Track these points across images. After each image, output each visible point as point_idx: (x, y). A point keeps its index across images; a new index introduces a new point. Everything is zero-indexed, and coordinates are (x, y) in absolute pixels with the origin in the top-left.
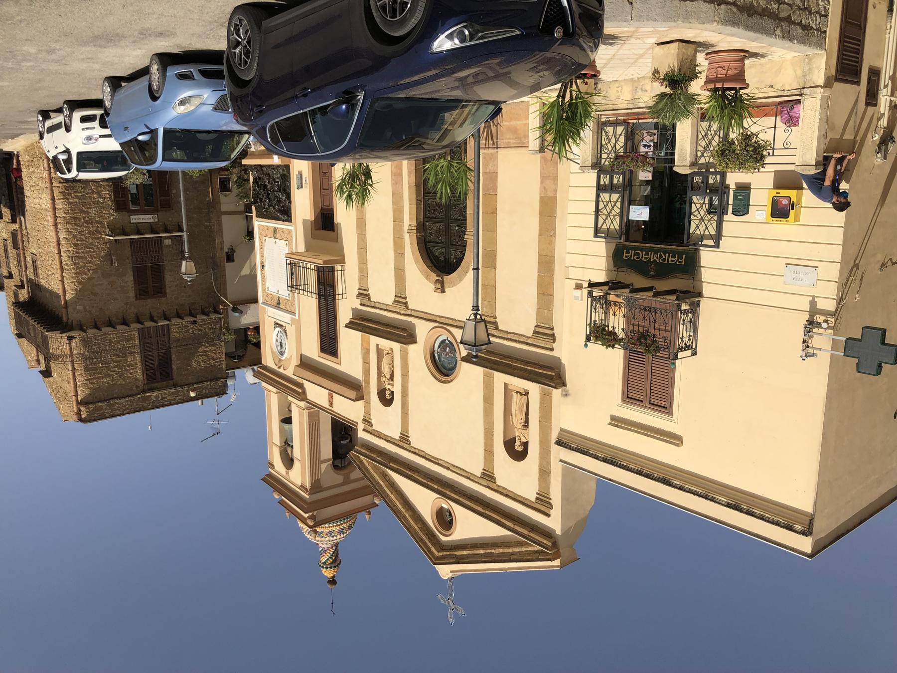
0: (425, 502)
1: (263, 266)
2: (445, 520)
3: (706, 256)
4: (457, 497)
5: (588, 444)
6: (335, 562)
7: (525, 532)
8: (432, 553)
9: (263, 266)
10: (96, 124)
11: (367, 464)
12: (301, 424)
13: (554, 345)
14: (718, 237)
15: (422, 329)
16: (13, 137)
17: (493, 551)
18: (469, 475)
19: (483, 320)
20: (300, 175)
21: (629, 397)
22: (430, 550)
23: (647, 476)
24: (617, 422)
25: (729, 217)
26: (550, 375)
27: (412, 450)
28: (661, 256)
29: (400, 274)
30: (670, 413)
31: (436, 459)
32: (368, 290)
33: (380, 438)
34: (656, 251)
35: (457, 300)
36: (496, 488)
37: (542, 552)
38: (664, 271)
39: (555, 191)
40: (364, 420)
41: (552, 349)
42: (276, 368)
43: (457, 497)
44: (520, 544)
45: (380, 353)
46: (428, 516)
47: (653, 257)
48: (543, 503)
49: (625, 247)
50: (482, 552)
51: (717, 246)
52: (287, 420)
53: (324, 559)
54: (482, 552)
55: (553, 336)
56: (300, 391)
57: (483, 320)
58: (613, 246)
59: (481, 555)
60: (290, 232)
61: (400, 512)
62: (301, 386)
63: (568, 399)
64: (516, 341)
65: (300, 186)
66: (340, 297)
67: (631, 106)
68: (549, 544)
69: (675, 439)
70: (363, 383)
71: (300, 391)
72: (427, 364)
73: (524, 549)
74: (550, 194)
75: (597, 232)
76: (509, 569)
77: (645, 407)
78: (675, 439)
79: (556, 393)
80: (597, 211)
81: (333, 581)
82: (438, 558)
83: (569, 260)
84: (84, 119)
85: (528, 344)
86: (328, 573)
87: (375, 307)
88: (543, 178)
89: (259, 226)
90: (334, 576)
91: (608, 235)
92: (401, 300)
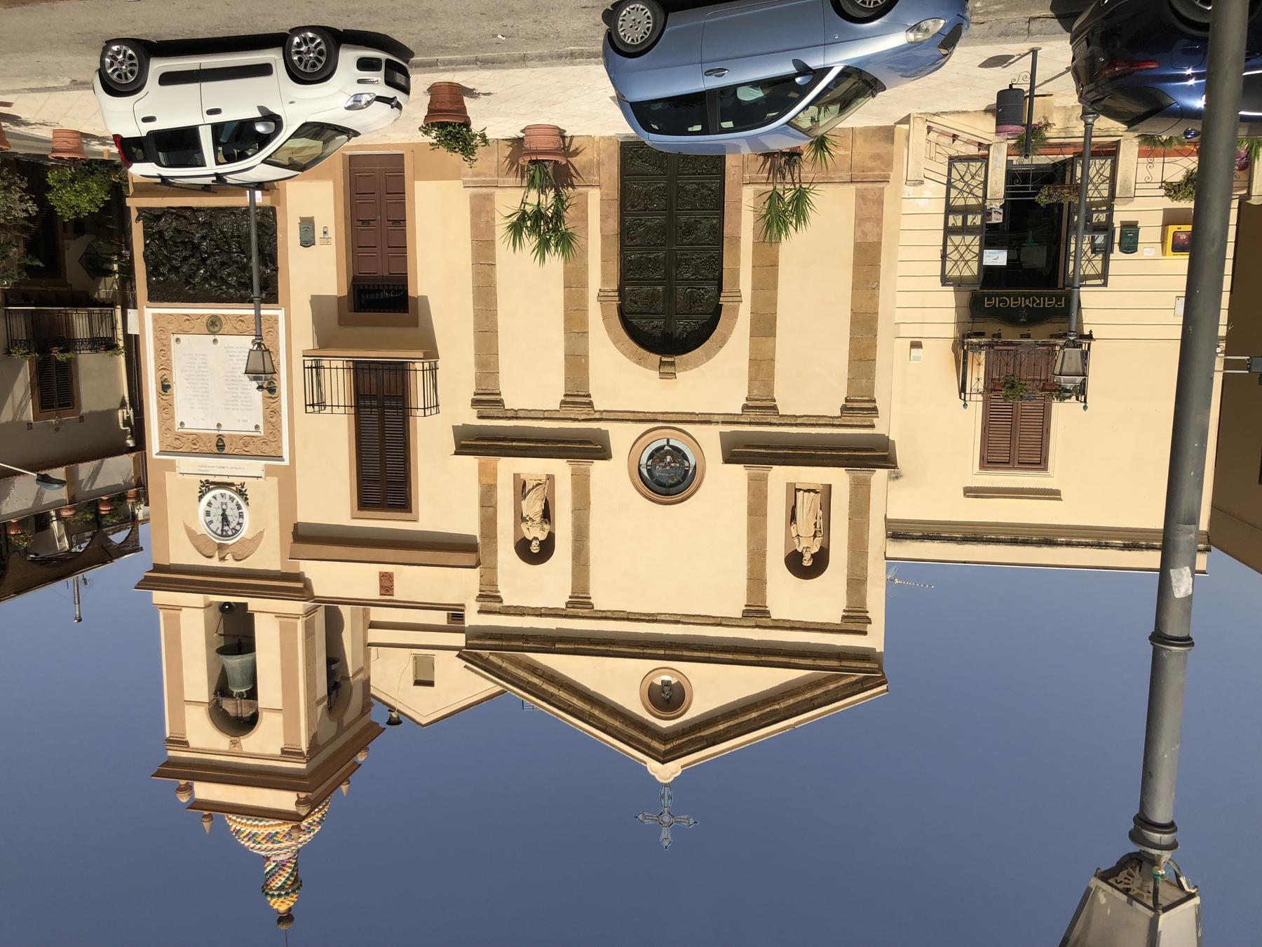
0: (622, 682)
1: (165, 387)
2: (668, 698)
3: (1089, 298)
4: (707, 655)
5: (935, 529)
6: (296, 883)
7: (835, 663)
8: (654, 750)
9: (165, 387)
10: (378, 76)
11: (498, 661)
12: (353, 629)
13: (875, 420)
14: (1104, 275)
15: (622, 437)
16: (486, 63)
17: (703, 734)
18: (718, 621)
19: (761, 405)
20: (307, 226)
21: (988, 462)
22: (649, 747)
23: (1025, 543)
24: (970, 492)
25: (1116, 254)
26: (873, 455)
27: (599, 615)
28: (1034, 301)
29: (576, 363)
30: (1045, 469)
31: (653, 615)
32: (499, 394)
33: (523, 615)
34: (1027, 296)
35: (713, 382)
36: (771, 624)
37: (865, 679)
38: (1036, 317)
39: (880, 235)
40: (482, 597)
41: (873, 426)
42: (215, 562)
43: (707, 655)
44: (829, 680)
45: (522, 489)
46: (634, 703)
47: (1023, 302)
48: (856, 619)
49: (984, 295)
50: (754, 715)
51: (1105, 284)
52: (793, 518)
53: (278, 882)
54: (754, 715)
55: (875, 409)
56: (300, 585)
57: (761, 405)
58: (966, 296)
59: (755, 719)
60: (276, 319)
61: (582, 711)
62: (298, 577)
63: (900, 481)
64: (812, 425)
65: (307, 242)
66: (421, 412)
67: (1063, 135)
68: (861, 669)
69: (1053, 494)
70: (479, 540)
71: (300, 585)
72: (634, 484)
73: (843, 682)
74: (871, 239)
75: (945, 280)
76: (797, 723)
77: (1014, 468)
78: (1053, 494)
79: (880, 475)
80: (944, 256)
81: (287, 918)
82: (666, 753)
83: (899, 316)
84: (364, 64)
85: (833, 425)
86: (281, 905)
87: (517, 418)
88: (860, 220)
89: (156, 318)
90: (290, 909)
91: (958, 283)
92: (577, 397)
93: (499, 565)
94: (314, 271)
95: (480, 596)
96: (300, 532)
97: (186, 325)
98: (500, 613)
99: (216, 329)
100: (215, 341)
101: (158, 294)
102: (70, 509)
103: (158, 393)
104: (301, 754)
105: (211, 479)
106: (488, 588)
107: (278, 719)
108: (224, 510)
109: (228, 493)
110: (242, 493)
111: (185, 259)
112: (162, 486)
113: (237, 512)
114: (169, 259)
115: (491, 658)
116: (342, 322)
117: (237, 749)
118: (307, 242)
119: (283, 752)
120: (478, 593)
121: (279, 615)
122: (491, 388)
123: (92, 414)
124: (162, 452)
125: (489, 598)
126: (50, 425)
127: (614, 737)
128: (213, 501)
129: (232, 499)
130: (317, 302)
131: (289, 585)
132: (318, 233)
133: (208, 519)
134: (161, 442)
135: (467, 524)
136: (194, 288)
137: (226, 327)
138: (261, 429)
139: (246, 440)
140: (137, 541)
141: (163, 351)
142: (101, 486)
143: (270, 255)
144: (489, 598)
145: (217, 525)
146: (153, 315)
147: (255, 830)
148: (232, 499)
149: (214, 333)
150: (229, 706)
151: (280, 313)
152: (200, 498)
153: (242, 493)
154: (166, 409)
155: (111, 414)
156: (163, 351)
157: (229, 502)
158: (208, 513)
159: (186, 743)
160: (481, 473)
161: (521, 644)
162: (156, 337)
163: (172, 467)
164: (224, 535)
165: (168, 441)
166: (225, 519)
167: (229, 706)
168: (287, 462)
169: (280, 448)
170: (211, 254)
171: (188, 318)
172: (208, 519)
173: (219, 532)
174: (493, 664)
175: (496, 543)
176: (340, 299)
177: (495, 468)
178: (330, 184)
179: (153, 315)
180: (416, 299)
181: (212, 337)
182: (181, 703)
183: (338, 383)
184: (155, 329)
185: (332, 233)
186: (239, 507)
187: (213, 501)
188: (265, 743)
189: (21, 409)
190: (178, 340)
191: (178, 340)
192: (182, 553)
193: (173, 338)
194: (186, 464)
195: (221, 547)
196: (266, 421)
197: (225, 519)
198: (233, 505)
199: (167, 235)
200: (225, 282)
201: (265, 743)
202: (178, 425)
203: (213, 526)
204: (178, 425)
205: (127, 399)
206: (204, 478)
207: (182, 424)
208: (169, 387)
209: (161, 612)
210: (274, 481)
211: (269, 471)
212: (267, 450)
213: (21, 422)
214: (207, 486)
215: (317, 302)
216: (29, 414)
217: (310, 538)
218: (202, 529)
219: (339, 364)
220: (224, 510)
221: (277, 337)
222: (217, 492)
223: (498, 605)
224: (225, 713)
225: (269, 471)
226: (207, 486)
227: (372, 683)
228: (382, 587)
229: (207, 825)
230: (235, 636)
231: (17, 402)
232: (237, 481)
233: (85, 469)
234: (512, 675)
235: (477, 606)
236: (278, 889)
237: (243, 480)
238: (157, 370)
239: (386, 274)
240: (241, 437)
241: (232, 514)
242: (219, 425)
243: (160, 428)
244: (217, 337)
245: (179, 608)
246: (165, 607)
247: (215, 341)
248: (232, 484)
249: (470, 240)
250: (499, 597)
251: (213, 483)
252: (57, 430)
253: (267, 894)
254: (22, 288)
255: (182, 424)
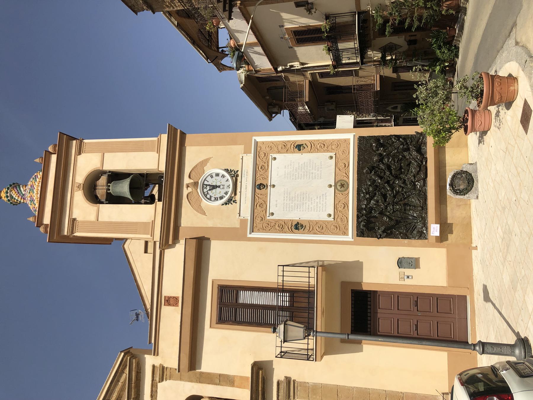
1: (299, 147)
9: (299, 147)
11: (122, 380)
40: (163, 369)
42: (187, 180)
56: (170, 243)
65: (401, 263)
89: (347, 141)
93: (182, 382)
94: (380, 265)
95: (163, 368)
96: (205, 242)
97: (341, 165)
98: (153, 380)
99: (339, 188)
100: (330, 186)
101: (363, 143)
102: (234, 45)
103: (295, 142)
104: (72, 233)
105: (239, 179)
106: (168, 373)
107: (93, 218)
108: (219, 187)
109: (230, 190)
110: (230, 201)
111: (389, 167)
112: (234, 142)
113: (218, 196)
114: (388, 155)
115: (124, 375)
116: (344, 284)
117: (76, 188)
118: (401, 263)
119: (74, 220)
120: (165, 366)
121: (153, 222)
122: (298, 393)
123: (295, 52)
124: (256, 143)
125: (161, 374)
126: (284, 35)
127: (109, 387)
128: (225, 179)
129: (226, 193)
130: (358, 266)
131: (171, 232)
132: (408, 271)
133: (214, 175)
134: (263, 143)
135: (209, 363)
136: (367, 173)
137: (339, 196)
138: (271, 217)
139: (264, 205)
140: (224, 70)
141: (323, 146)
142: (252, 56)
143: (391, 233)
144: (161, 374)
145: (211, 181)
146: (349, 139)
147: (35, 191)
148: (226, 193)
149: (335, 186)
150: (103, 180)
151: (350, 237)
152: (227, 170)
153: (230, 201)
154: (285, 148)
155: (296, 59)
156: (323, 146)
157: (224, 191)
158: (217, 175)
159: (80, 154)
160: (242, 378)
161: (133, 396)
162: (334, 141)
163: (247, 151)
164: (204, 186)
165: (263, 147)
166: (214, 187)
167: (103, 180)
168: (249, 236)
169: (259, 231)
170: (392, 188)
171: (347, 166)
172: (214, 175)
173: (206, 183)
174: (120, 376)
175: (197, 382)
176: (360, 284)
177: (244, 388)
178: (445, 284)
179: (349, 139)
180: (360, 342)
181: (333, 184)
182: (103, 151)
183: (300, 279)
184: (339, 140)
185: (408, 282)
186: (221, 198)
187: (225, 179)
188: (80, 208)
189: (291, 22)
190: (331, 157)
191: (331, 157)
192: (193, 154)
193: (333, 154)
194: (249, 160)
195: (196, 184)
196: (276, 221)
197: (214, 187)
198: (222, 194)
199: (406, 154)
200: (371, 198)
201: (80, 208)
202: (274, 155)
203: (209, 178)
204: (274, 155)
205: (306, 66)
206: (239, 173)
207: (275, 159)
208: (300, 150)
209: (155, 139)
210: (238, 225)
211: (243, 222)
212: (258, 221)
213: (283, 22)
214: (234, 175)
215: (358, 266)
216: (288, 26)
217: (200, 247)
218: (209, 170)
219: (313, 282)
220: (219, 187)
221: (333, 234)
222: (230, 183)
223: (158, 379)
224: (98, 178)
225: (243, 222)
226: (234, 175)
227: (245, 21)
228: (169, 298)
229: (37, 160)
230: (141, 188)
231: (296, 20)
232: (237, 198)
233: (259, 49)
234: (113, 389)
235: (157, 364)
236: (11, 195)
237: (238, 202)
238: (311, 142)
239: (379, 315)
240: (265, 202)
241: (214, 193)
242: (274, 186)
243: (272, 142)
244: (333, 188)
245: (158, 152)
246: (159, 142)
247: (330, 186)
248: (235, 194)
249: (404, 391)
250: (162, 380)
251: (236, 180)
252: (282, 38)
253: (8, 188)
254: (371, 19)
255: (275, 159)
